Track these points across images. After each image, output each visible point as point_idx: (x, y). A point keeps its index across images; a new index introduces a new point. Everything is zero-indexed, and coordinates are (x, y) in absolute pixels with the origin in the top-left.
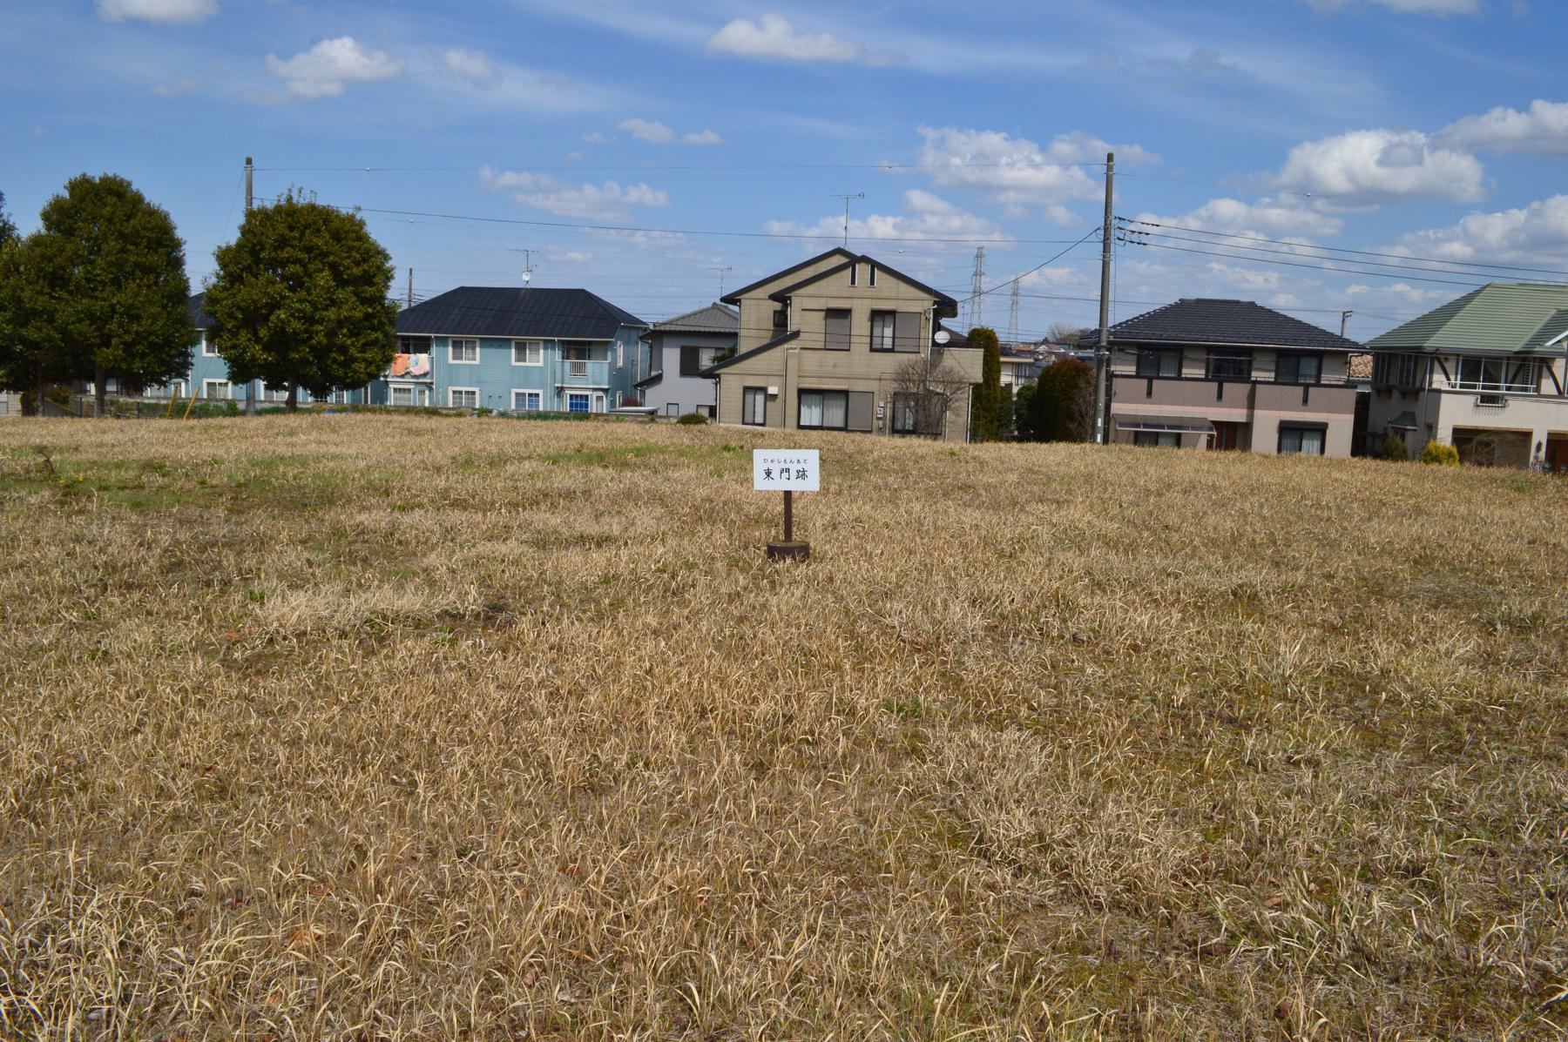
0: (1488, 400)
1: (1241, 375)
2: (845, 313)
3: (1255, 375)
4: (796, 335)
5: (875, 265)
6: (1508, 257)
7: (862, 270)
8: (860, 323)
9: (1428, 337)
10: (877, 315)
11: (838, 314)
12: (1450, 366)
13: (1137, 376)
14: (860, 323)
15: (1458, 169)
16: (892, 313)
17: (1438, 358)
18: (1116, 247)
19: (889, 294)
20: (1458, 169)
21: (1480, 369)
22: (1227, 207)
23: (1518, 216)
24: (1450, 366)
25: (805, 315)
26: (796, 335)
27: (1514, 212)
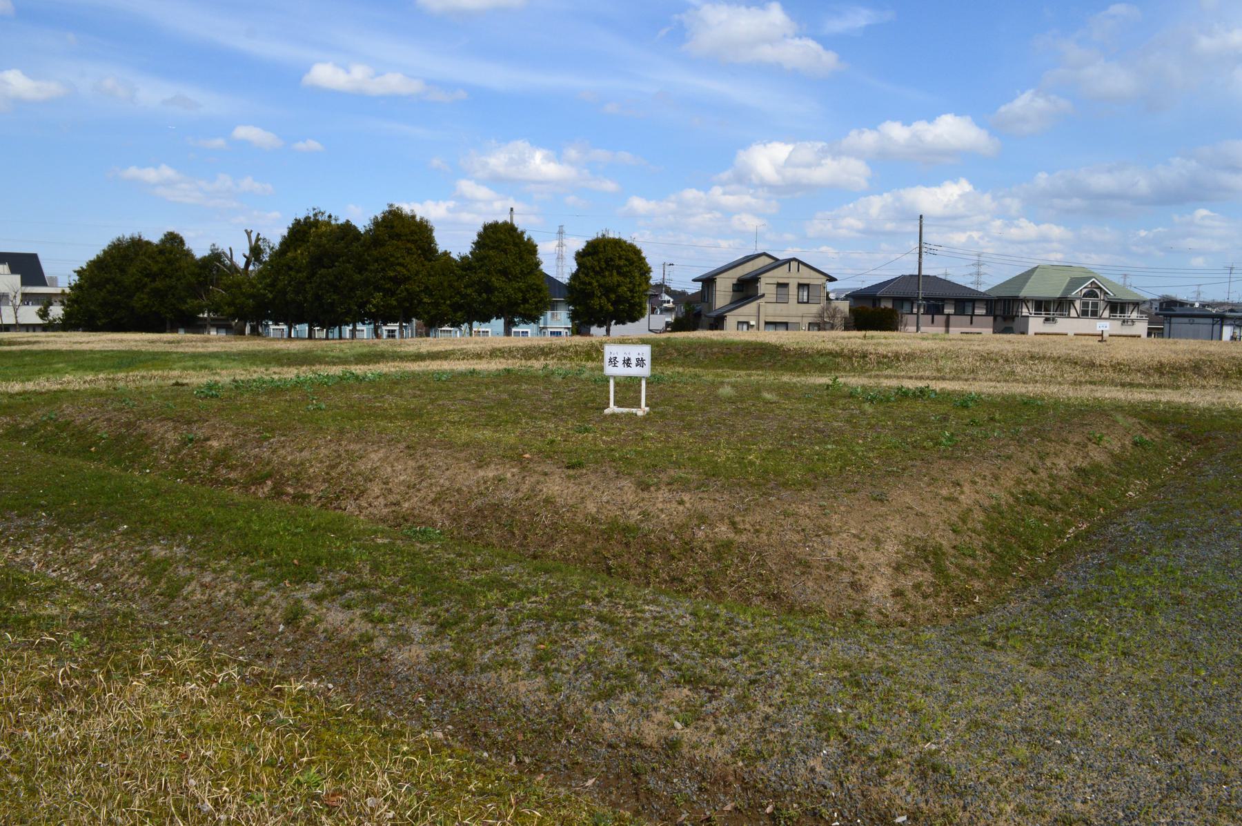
0: (1047, 320)
1: (939, 311)
2: (786, 285)
3: (946, 311)
4: (763, 296)
5: (799, 262)
6: (890, 226)
7: (794, 264)
8: (793, 289)
9: (1021, 288)
10: (801, 286)
11: (783, 286)
12: (1030, 305)
13: (986, 315)
14: (793, 289)
15: (853, 170)
16: (808, 285)
17: (1025, 301)
18: (924, 255)
19: (807, 276)
20: (853, 170)
21: (1041, 305)
22: (691, 194)
23: (888, 197)
24: (1030, 305)
25: (766, 285)
26: (763, 296)
27: (885, 195)
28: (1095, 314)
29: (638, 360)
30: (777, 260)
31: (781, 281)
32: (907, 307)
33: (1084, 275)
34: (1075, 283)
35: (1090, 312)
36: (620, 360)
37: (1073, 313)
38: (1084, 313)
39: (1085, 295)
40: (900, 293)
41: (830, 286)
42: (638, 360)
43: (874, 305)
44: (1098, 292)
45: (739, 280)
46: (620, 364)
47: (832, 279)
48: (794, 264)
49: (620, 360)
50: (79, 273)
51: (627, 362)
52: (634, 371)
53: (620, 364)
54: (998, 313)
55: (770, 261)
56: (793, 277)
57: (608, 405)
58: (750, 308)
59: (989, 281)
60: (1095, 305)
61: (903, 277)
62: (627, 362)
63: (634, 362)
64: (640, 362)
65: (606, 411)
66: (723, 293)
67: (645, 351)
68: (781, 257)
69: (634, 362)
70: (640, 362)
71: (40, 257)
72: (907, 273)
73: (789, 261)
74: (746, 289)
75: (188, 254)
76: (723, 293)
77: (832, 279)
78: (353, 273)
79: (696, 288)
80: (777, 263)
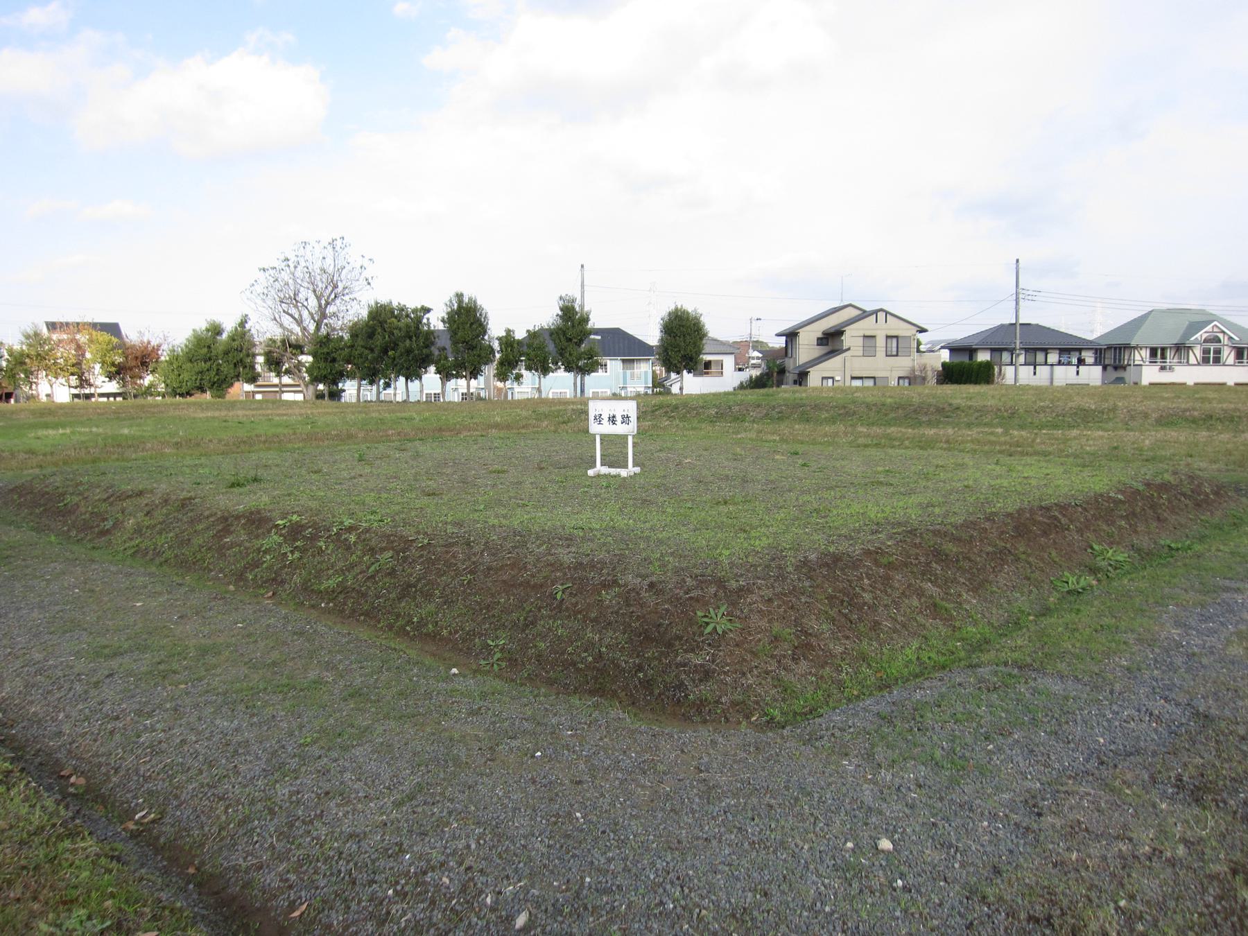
0: (1163, 368)
5: (887, 313)
7: (881, 316)
8: (881, 342)
14: (881, 342)
16: (897, 337)
25: (851, 338)
28: (1217, 361)
29: (623, 417)
30: (864, 311)
31: (868, 333)
32: (1006, 357)
33: (1205, 319)
34: (1195, 327)
35: (1212, 357)
36: (605, 417)
37: (1192, 360)
38: (1205, 361)
39: (1206, 341)
40: (997, 342)
41: (920, 336)
42: (623, 417)
43: (971, 358)
44: (1221, 336)
45: (824, 333)
46: (605, 421)
47: (922, 330)
48: (881, 316)
49: (605, 417)
50: (377, 303)
51: (612, 420)
52: (620, 429)
53: (605, 421)
54: (1107, 362)
55: (859, 312)
56: (881, 329)
57: (593, 465)
58: (836, 361)
59: (1093, 326)
60: (1218, 352)
61: (1002, 326)
62: (612, 420)
63: (619, 419)
64: (626, 419)
65: (591, 472)
66: (806, 348)
67: (631, 408)
68: (868, 308)
69: (619, 419)
70: (626, 419)
71: (121, 326)
72: (1007, 322)
73: (876, 312)
74: (831, 340)
75: (1095, 387)
76: (806, 348)
77: (922, 330)
78: (390, 343)
79: (781, 342)
80: (864, 315)
